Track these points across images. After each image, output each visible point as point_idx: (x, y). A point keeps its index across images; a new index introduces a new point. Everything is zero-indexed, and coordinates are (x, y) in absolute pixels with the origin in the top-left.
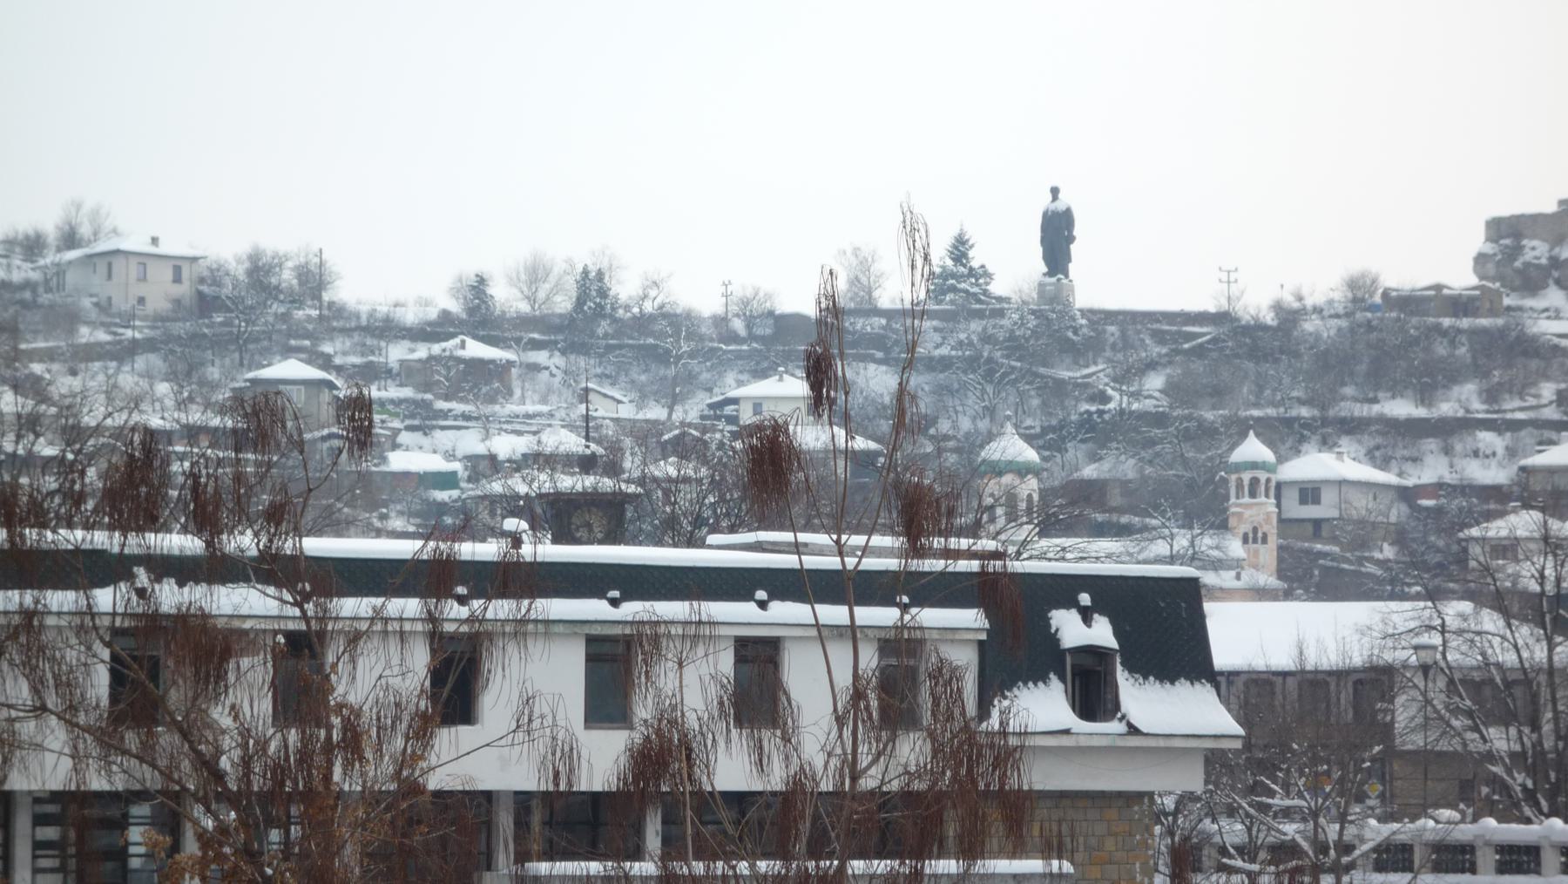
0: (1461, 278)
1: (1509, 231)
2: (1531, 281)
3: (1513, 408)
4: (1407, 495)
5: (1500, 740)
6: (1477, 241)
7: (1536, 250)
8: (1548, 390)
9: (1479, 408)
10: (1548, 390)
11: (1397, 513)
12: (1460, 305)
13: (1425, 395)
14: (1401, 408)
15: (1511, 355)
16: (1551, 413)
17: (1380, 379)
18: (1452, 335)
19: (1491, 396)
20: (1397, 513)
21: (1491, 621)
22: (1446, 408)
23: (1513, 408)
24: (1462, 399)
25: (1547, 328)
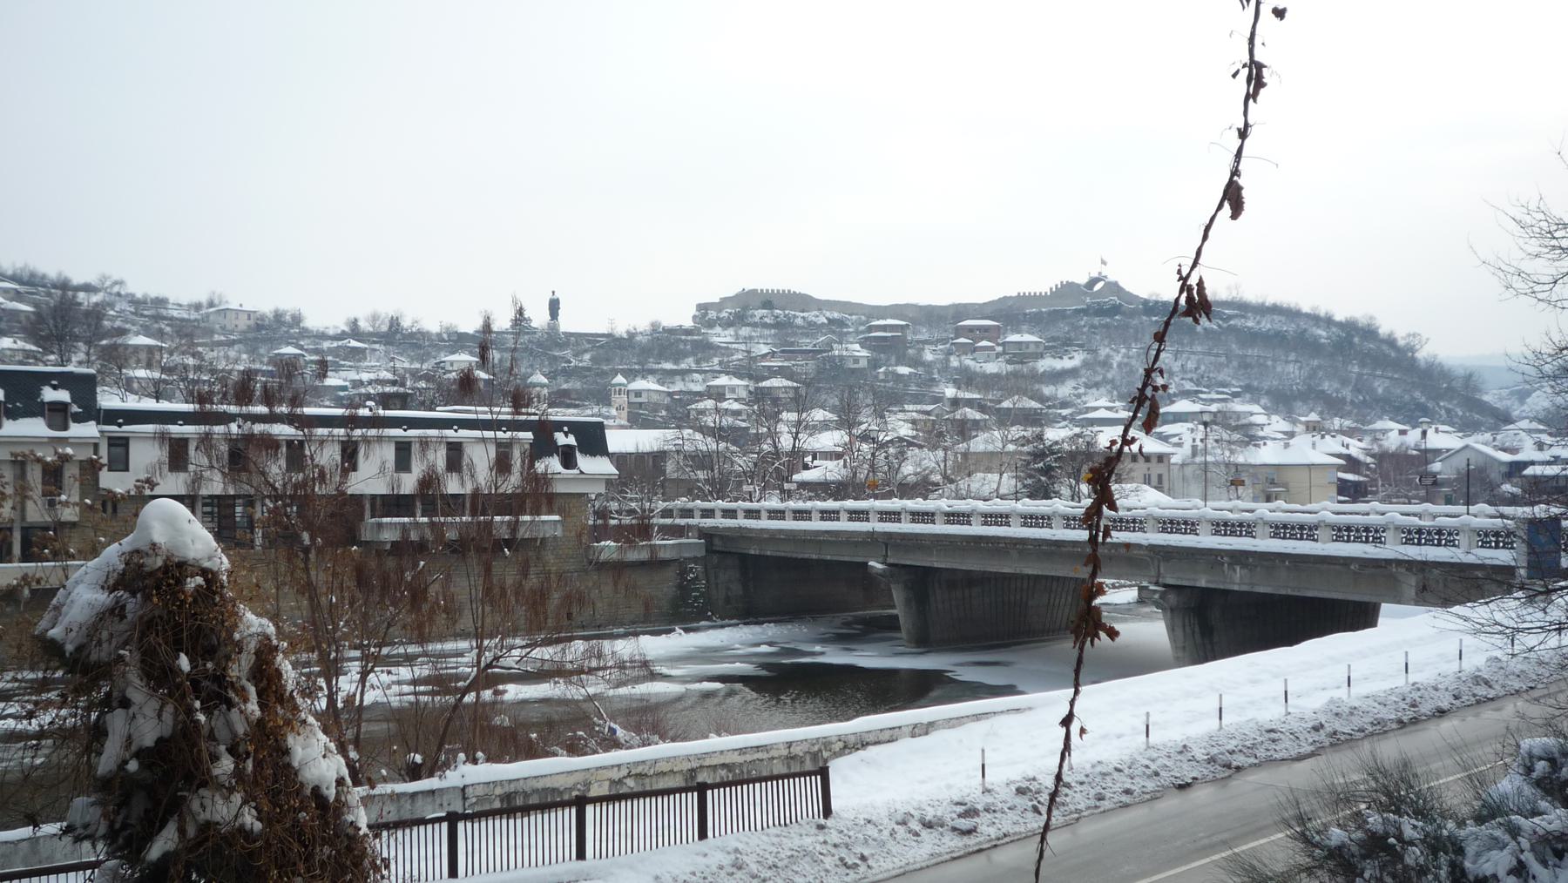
0: (688, 323)
1: (704, 308)
2: (711, 324)
3: (705, 366)
4: (670, 394)
5: (701, 475)
6: (693, 311)
7: (712, 314)
8: (716, 360)
9: (694, 366)
10: (716, 360)
11: (667, 400)
12: (688, 332)
13: (676, 362)
14: (668, 366)
15: (704, 349)
16: (717, 368)
17: (662, 356)
18: (685, 342)
19: (698, 362)
20: (667, 400)
21: (698, 436)
22: (683, 366)
23: (705, 366)
24: (688, 363)
25: (716, 340)
